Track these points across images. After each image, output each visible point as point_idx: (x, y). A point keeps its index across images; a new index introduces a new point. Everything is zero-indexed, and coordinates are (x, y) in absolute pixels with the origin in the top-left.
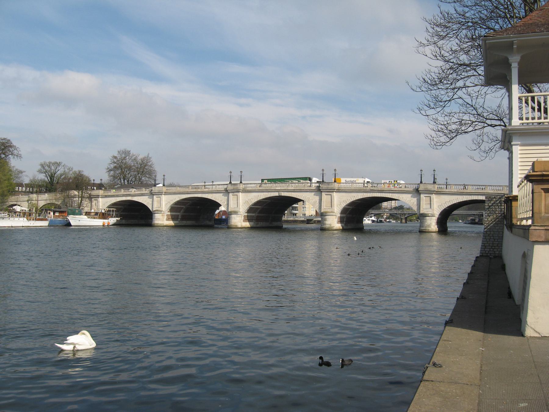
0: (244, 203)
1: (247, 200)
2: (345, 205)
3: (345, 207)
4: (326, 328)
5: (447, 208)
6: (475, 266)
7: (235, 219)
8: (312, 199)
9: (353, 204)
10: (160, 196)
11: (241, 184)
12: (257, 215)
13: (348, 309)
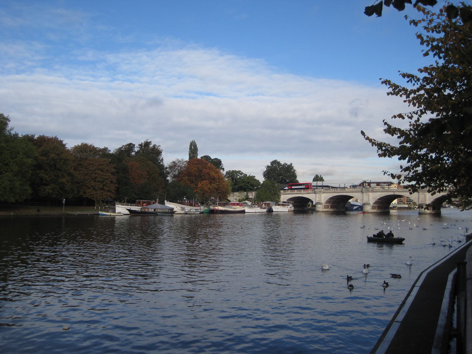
0: (373, 199)
1: (374, 197)
2: (433, 200)
3: (328, 200)
4: (84, 315)
5: (434, 201)
6: (435, 245)
7: (367, 208)
8: (414, 197)
9: (331, 198)
10: (320, 194)
11: (370, 188)
12: (378, 205)
13: (375, 268)
